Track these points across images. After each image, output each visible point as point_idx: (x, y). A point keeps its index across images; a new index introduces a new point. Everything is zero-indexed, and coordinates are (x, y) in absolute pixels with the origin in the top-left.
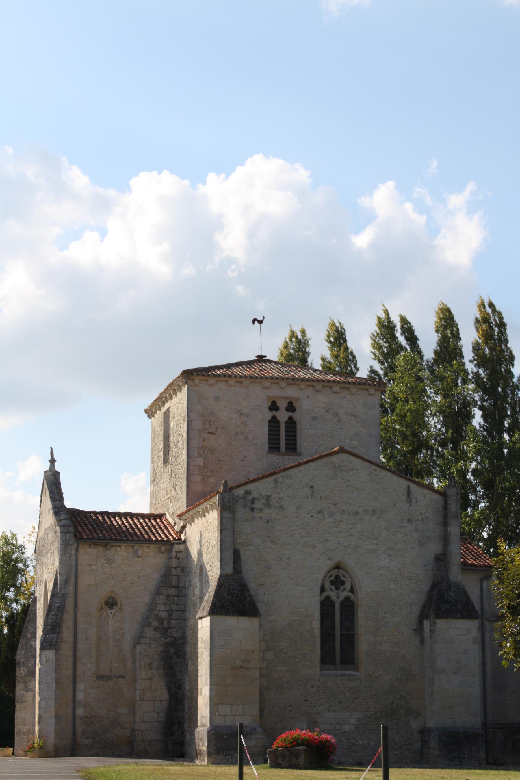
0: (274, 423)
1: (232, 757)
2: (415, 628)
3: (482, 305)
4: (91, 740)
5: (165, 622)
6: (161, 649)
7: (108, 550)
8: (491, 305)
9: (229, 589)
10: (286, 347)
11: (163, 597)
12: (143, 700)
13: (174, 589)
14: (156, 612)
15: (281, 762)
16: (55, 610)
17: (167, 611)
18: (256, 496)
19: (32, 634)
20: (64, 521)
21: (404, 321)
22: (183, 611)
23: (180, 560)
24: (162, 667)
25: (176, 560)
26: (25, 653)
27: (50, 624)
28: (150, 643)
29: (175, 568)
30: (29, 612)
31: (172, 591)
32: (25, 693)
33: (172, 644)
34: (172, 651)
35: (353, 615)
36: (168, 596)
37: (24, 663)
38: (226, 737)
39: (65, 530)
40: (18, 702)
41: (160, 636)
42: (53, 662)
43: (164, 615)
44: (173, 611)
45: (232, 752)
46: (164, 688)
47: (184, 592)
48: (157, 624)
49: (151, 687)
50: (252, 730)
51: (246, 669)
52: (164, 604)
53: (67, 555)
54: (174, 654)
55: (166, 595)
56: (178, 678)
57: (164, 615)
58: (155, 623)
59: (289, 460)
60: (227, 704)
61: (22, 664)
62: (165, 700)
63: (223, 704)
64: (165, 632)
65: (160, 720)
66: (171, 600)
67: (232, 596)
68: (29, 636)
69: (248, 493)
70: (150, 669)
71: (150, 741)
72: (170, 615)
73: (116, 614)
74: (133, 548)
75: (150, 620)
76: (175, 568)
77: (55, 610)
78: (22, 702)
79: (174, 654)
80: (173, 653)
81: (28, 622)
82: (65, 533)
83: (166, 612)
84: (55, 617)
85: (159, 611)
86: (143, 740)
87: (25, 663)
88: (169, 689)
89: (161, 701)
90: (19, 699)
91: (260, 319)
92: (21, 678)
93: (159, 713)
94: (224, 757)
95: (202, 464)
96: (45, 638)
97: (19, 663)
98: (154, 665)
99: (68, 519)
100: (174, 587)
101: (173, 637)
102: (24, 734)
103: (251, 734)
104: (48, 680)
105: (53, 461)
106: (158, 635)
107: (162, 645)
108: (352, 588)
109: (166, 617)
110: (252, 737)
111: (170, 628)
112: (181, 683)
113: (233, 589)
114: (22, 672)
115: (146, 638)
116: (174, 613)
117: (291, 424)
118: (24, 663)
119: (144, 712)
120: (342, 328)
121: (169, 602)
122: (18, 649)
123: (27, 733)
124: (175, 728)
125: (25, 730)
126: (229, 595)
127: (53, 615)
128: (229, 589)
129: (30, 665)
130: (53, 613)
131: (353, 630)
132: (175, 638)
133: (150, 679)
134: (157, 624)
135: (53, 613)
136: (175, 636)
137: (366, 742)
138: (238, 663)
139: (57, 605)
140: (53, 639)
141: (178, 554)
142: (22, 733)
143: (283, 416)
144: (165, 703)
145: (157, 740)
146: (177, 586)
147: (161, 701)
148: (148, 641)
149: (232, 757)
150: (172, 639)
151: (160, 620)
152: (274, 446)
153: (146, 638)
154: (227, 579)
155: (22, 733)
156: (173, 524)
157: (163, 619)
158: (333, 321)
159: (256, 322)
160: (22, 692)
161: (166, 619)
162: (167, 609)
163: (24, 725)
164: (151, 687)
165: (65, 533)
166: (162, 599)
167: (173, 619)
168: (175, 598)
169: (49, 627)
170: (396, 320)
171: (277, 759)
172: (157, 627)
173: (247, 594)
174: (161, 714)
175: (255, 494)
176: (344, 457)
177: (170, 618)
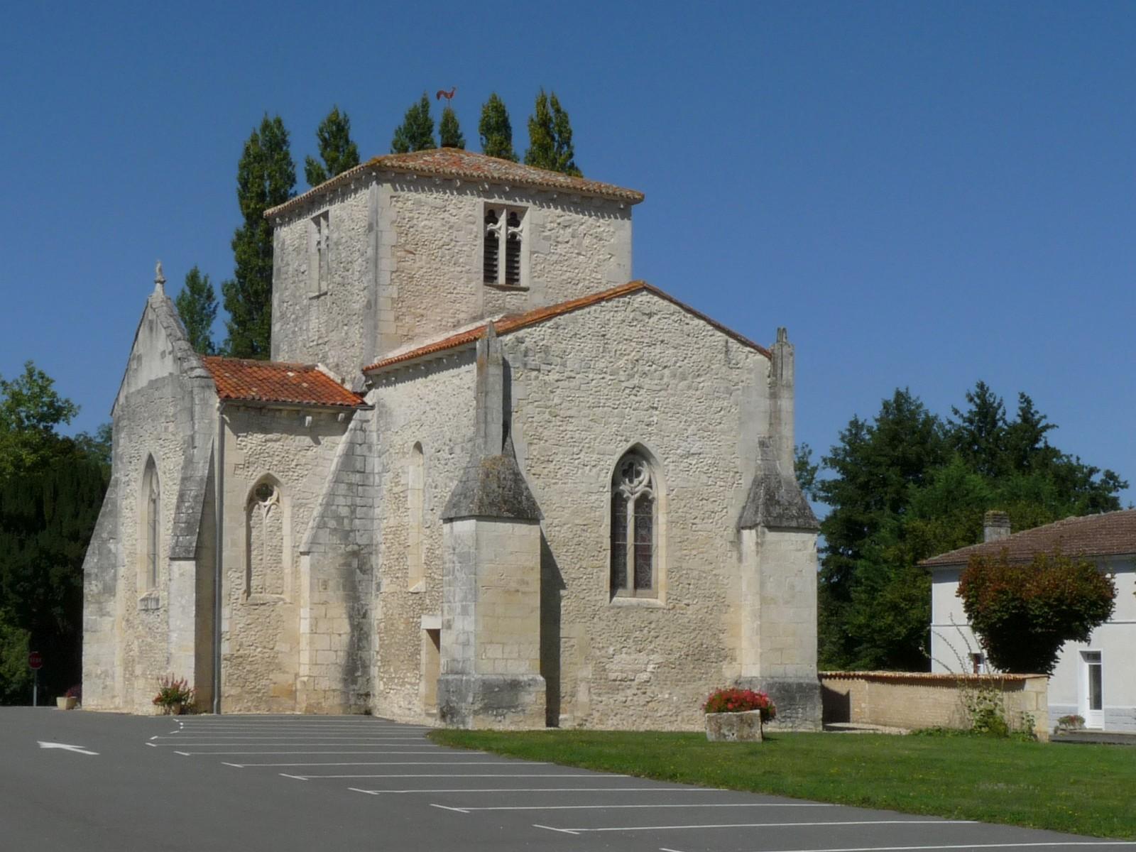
0: (491, 242)
1: (504, 718)
2: (732, 539)
3: (542, 103)
4: (239, 690)
5: (346, 521)
6: (341, 560)
7: (264, 415)
8: (555, 104)
9: (499, 478)
10: (254, 140)
11: (343, 486)
12: (316, 633)
13: (358, 475)
14: (334, 507)
15: (727, 733)
16: (191, 500)
17: (349, 506)
18: (530, 346)
19: (109, 533)
20: (198, 370)
22: (371, 507)
23: (367, 433)
24: (341, 586)
25: (362, 433)
26: (99, 560)
27: (184, 520)
28: (325, 552)
29: (360, 445)
30: (105, 500)
31: (356, 478)
32: (98, 619)
33: (355, 554)
34: (355, 563)
35: (650, 519)
36: (350, 485)
37: (97, 575)
38: (497, 689)
39: (203, 384)
40: (87, 631)
41: (338, 542)
42: (192, 576)
43: (344, 511)
44: (357, 506)
45: (505, 711)
46: (344, 616)
47: (372, 480)
48: (335, 526)
49: (326, 615)
50: (531, 680)
51: (524, 593)
52: (345, 496)
53: (207, 421)
54: (358, 568)
55: (347, 483)
56: (363, 602)
57: (344, 511)
58: (332, 524)
60: (497, 643)
61: (93, 576)
62: (345, 633)
63: (491, 643)
64: (346, 535)
65: (338, 661)
66: (354, 490)
67: (504, 488)
68: (105, 535)
69: (520, 341)
70: (325, 589)
71: (325, 691)
72: (353, 512)
73: (272, 507)
74: (298, 414)
75: (326, 519)
76: (360, 445)
77: (191, 500)
78: (95, 632)
79: (358, 568)
80: (356, 566)
81: (103, 516)
82: (203, 387)
83: (347, 508)
84: (191, 511)
85: (338, 506)
86: (315, 690)
87: (99, 574)
88: (351, 617)
89: (340, 635)
90: (89, 626)
91: (449, 91)
92: (92, 596)
93: (336, 651)
94: (493, 718)
95: (395, 296)
96: (177, 541)
97: (89, 575)
98: (331, 583)
99: (202, 367)
100: (358, 472)
101: (357, 544)
102: (98, 677)
103: (530, 685)
104: (184, 602)
105: (266, 114)
106: (335, 540)
107: (342, 555)
108: (650, 482)
109: (348, 514)
110: (531, 689)
111: (352, 531)
112: (366, 611)
113: (504, 478)
114: (94, 588)
115: (320, 544)
116: (358, 508)
117: (514, 245)
118: (97, 575)
119: (317, 651)
120: (347, 121)
121: (351, 494)
122: (87, 554)
123: (103, 676)
124: (359, 674)
125: (99, 672)
126: (499, 487)
127: (188, 508)
128: (499, 478)
129: (107, 578)
130: (187, 504)
131: (650, 540)
132: (359, 546)
133: (325, 603)
134: (335, 526)
135: (187, 504)
136: (360, 542)
137: (667, 696)
138: (513, 585)
139: (193, 493)
140: (191, 543)
141: (364, 425)
142: (94, 675)
143: (502, 229)
144: (345, 639)
145: (334, 690)
146: (362, 470)
147: (340, 635)
148: (322, 549)
149: (504, 718)
150: (356, 548)
151: (339, 519)
153: (320, 544)
154: (494, 464)
155: (94, 675)
156: (339, 381)
157: (343, 518)
158: (337, 111)
159: (442, 96)
160: (94, 617)
161: (347, 517)
162: (349, 504)
163: (98, 664)
164: (326, 615)
165: (203, 387)
166: (342, 488)
167: (356, 518)
168: (360, 488)
169: (183, 525)
170: (271, 120)
171: (720, 728)
172: (335, 529)
173: (523, 486)
174: (339, 653)
175: (529, 342)
176: (644, 297)
177: (353, 517)
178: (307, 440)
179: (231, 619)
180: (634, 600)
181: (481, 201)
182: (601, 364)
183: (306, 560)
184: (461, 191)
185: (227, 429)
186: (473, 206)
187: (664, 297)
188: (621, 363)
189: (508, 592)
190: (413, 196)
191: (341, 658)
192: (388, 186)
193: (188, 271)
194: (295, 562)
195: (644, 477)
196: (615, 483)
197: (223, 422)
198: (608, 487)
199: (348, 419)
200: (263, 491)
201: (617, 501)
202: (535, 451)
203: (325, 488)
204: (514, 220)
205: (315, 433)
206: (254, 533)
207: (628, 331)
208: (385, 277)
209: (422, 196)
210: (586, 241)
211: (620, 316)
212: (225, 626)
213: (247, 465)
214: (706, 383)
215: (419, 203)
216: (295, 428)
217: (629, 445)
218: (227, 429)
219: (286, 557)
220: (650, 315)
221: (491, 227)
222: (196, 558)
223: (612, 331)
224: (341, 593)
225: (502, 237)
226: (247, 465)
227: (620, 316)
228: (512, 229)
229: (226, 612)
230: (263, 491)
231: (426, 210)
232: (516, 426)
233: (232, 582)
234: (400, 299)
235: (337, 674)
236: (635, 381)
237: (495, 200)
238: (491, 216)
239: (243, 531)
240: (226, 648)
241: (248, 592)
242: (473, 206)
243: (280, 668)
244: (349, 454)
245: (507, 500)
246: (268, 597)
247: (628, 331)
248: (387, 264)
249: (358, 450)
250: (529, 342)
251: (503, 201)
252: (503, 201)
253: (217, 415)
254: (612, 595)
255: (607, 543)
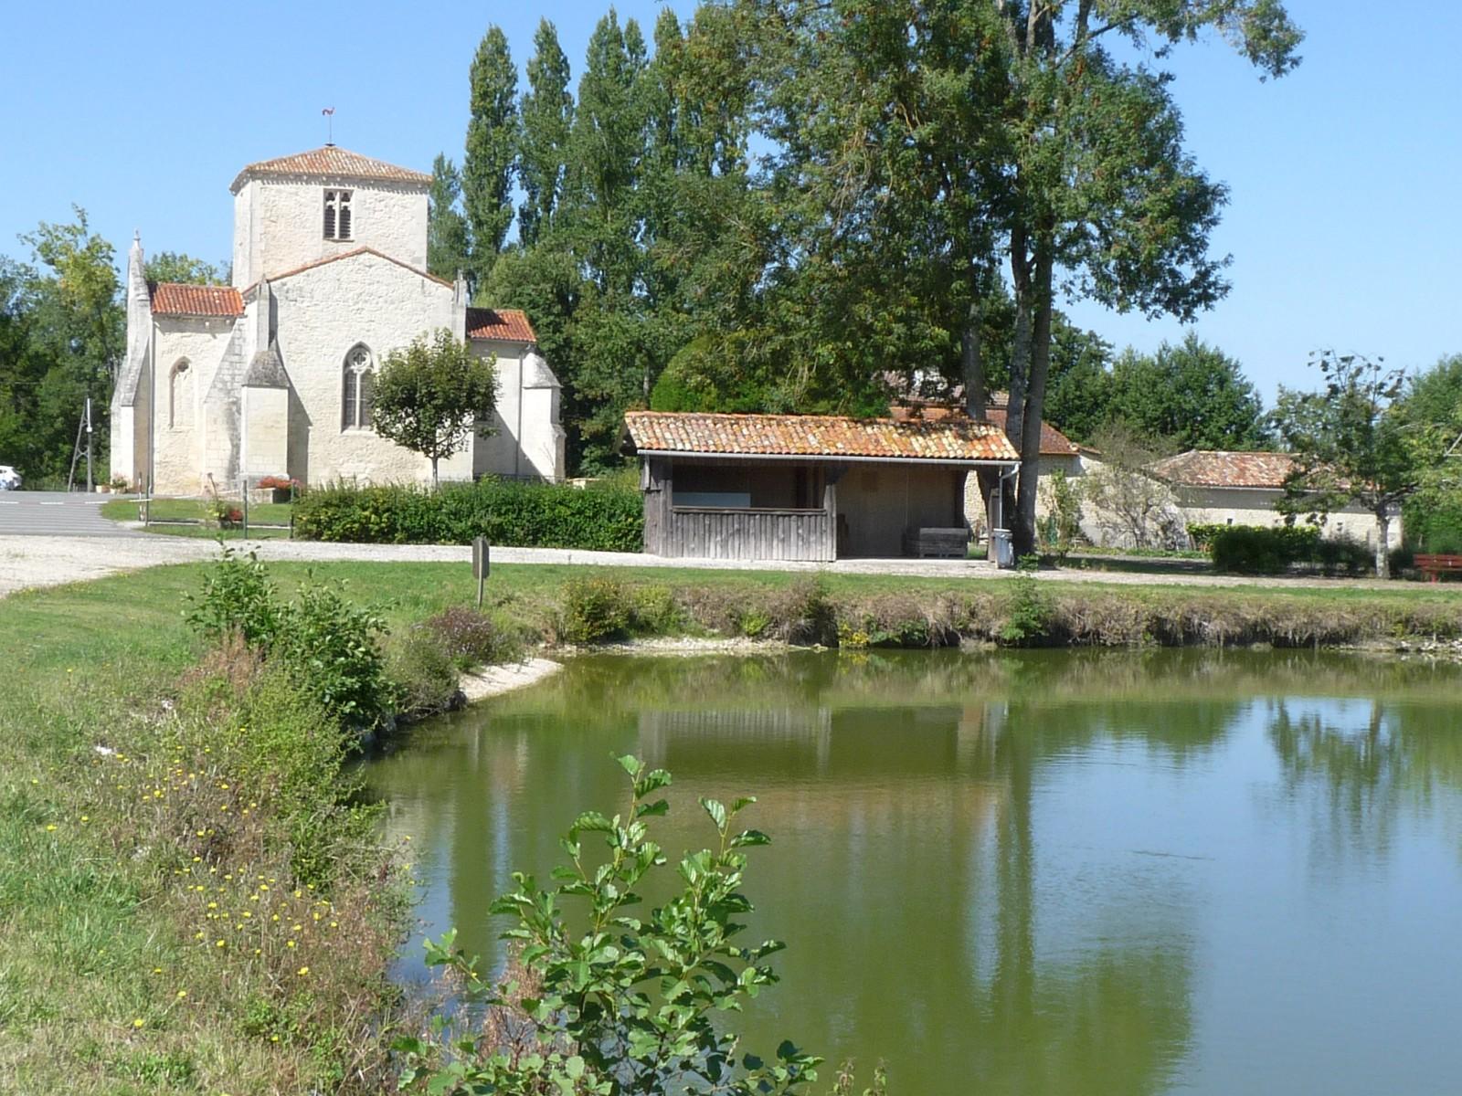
0: (329, 213)
21: (632, 27)
31: (236, 358)
34: (234, 408)
43: (227, 378)
57: (227, 378)
58: (220, 385)
59: (343, 248)
88: (231, 440)
98: (219, 420)
117: (345, 214)
120: (553, 28)
138: (270, 424)
143: (337, 205)
151: (225, 383)
152: (328, 232)
175: (289, 285)
176: (367, 255)
178: (208, 336)
179: (161, 440)
180: (358, 433)
181: (323, 187)
182: (337, 297)
183: (205, 406)
184: (307, 182)
185: (157, 331)
186: (317, 191)
187: (380, 256)
188: (351, 295)
189: (266, 427)
190: (275, 187)
191: (226, 464)
192: (259, 182)
193: (435, 156)
194: (201, 408)
195: (368, 361)
196: (347, 364)
197: (154, 326)
198: (341, 368)
199: (233, 324)
200: (182, 366)
201: (348, 377)
202: (292, 347)
203: (216, 365)
204: (346, 197)
205: (213, 331)
206: (176, 391)
207: (355, 277)
208: (257, 238)
209: (281, 187)
210: (396, 209)
211: (350, 268)
212: (156, 444)
213: (170, 351)
214: (408, 306)
215: (279, 191)
216: (200, 329)
217: (354, 344)
218: (157, 331)
219: (196, 405)
220: (370, 266)
221: (330, 203)
222: (134, 405)
223: (344, 277)
224: (225, 426)
225: (337, 209)
226: (170, 351)
227: (350, 268)
228: (344, 204)
229: (156, 436)
230: (182, 366)
231: (284, 195)
232: (280, 334)
233: (161, 419)
234: (267, 251)
235: (224, 473)
236: (359, 306)
237: (332, 187)
238: (330, 196)
239: (168, 389)
240: (157, 458)
241: (172, 425)
242: (317, 191)
243: (191, 469)
244: (232, 344)
245: (271, 375)
246: (184, 428)
247: (355, 277)
248: (258, 229)
249: (237, 342)
250: (289, 285)
251: (337, 187)
252: (337, 187)
253: (151, 322)
254: (343, 430)
255: (339, 399)
